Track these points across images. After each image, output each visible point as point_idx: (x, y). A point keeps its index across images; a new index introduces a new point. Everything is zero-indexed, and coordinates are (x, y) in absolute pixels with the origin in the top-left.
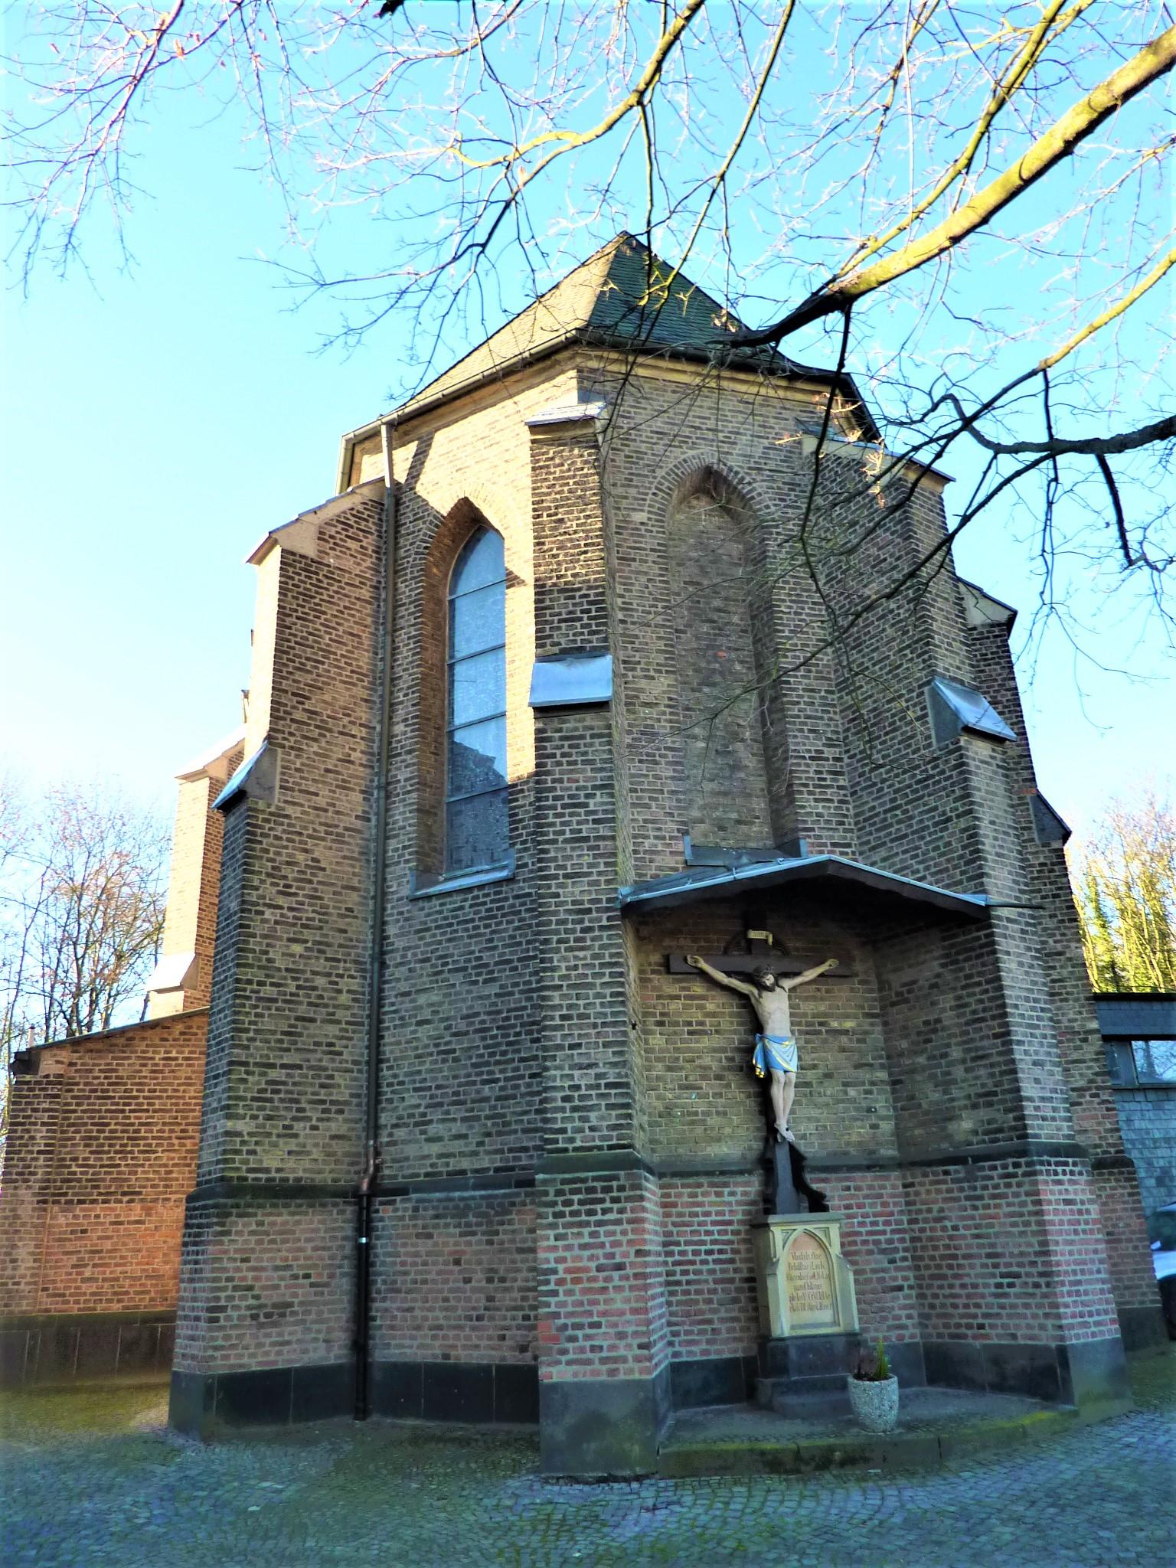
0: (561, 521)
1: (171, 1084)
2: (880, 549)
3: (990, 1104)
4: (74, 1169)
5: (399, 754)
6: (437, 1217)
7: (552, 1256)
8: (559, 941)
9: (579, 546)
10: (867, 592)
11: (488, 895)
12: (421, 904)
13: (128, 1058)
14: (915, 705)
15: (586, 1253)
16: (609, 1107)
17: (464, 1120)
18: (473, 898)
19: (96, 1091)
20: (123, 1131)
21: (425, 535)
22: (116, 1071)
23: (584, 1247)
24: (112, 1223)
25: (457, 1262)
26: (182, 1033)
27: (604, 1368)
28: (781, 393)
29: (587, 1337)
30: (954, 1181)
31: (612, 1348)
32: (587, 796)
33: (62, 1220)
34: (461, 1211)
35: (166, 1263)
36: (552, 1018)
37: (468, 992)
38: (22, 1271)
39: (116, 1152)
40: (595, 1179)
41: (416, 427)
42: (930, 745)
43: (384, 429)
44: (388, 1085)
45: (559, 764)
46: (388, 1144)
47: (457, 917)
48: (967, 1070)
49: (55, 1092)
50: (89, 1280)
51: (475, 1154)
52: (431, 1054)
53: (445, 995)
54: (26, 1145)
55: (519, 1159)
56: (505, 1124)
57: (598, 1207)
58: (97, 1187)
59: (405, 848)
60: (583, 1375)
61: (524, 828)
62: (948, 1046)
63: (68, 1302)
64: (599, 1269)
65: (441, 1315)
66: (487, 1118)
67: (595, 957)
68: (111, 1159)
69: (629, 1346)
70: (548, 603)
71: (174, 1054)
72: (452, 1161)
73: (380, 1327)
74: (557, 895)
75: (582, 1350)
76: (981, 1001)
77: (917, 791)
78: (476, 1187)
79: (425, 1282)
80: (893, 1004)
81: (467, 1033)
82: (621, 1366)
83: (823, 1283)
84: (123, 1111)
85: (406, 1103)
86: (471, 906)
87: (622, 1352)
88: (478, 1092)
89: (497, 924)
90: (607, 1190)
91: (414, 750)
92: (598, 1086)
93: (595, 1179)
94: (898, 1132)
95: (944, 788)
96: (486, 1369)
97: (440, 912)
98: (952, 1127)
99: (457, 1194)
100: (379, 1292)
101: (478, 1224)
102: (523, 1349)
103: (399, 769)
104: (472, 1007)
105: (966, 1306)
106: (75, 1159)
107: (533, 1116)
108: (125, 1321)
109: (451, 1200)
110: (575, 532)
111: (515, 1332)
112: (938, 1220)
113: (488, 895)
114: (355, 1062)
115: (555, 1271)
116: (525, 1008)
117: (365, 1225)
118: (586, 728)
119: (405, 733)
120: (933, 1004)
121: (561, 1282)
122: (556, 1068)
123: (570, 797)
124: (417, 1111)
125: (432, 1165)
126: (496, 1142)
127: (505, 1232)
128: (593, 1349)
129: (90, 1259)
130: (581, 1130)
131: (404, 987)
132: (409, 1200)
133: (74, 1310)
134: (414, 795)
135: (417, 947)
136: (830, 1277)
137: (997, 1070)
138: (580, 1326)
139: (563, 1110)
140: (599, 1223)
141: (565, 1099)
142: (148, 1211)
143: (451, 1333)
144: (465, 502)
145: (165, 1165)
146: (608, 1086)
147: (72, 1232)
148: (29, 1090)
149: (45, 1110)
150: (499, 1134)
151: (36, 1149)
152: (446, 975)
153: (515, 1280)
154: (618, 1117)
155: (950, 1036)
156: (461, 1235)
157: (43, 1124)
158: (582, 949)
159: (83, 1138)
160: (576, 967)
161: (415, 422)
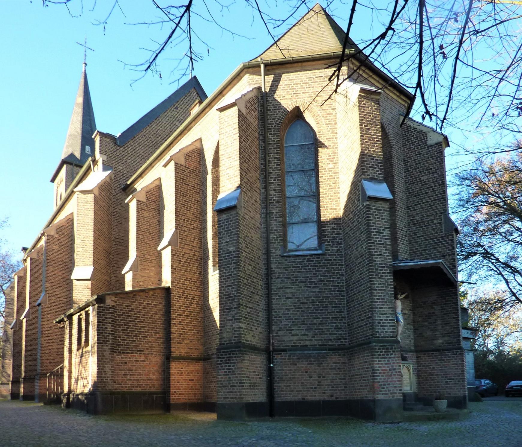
0: (368, 129)
1: (150, 313)
2: (430, 165)
3: (449, 336)
4: (120, 341)
5: (273, 203)
6: (299, 359)
7: (378, 366)
8: (376, 275)
9: (374, 141)
10: (422, 178)
11: (314, 258)
12: (286, 258)
13: (135, 302)
14: (438, 219)
15: (387, 365)
16: (391, 326)
17: (306, 330)
18: (308, 259)
19: (124, 313)
20: (136, 329)
21: (280, 117)
22: (130, 306)
23: (386, 364)
25: (307, 372)
26: (153, 295)
27: (391, 395)
28: (395, 97)
29: (387, 388)
30: (435, 356)
31: (393, 390)
32: (383, 230)
33: (118, 359)
34: (307, 357)
35: (153, 375)
36: (374, 299)
37: (307, 290)
38: (108, 375)
40: (388, 345)
41: (274, 69)
42: (442, 232)
43: (262, 66)
45: (375, 218)
46: (276, 336)
48: (442, 327)
51: (311, 340)
52: (293, 308)
53: (297, 290)
54: (104, 331)
55: (328, 342)
56: (322, 332)
57: (389, 353)
58: (129, 348)
59: (277, 237)
60: (386, 397)
61: (328, 237)
63: (122, 387)
64: (390, 370)
66: (316, 329)
67: (386, 281)
68: (132, 338)
69: (397, 390)
70: (365, 159)
71: (150, 303)
72: (302, 342)
73: (277, 391)
74: (375, 261)
75: (386, 391)
76: (450, 308)
77: (435, 246)
78: (313, 350)
79: (294, 378)
80: (418, 307)
81: (307, 303)
82: (395, 395)
83: (408, 380)
84: (135, 321)
85: (283, 324)
86: (307, 261)
87: (395, 391)
88: (312, 321)
89: (318, 269)
90: (392, 349)
91: (280, 202)
92: (387, 320)
93: (388, 345)
94: (415, 343)
95: (445, 246)
96: (319, 402)
97: (295, 262)
98: (435, 342)
100: (276, 381)
101: (314, 361)
104: (308, 295)
105: (434, 387)
106: (120, 337)
107: (333, 330)
108: (143, 394)
109: (304, 354)
110: (373, 135)
111: (329, 391)
112: (428, 366)
113: (314, 258)
114: (263, 309)
115: (378, 370)
116: (330, 297)
117: (270, 360)
118: (382, 207)
119: (275, 195)
120: (433, 308)
121: (380, 373)
122: (376, 314)
123: (378, 229)
124: (287, 326)
125: (294, 343)
126: (320, 337)
127: (325, 363)
128: (389, 390)
129: (129, 373)
130: (383, 332)
131: (279, 286)
132: (286, 354)
133: (125, 389)
134: (281, 219)
135: (285, 273)
136: (410, 378)
137: (452, 327)
138: (385, 385)
139: (378, 326)
140: (390, 358)
141: (379, 323)
142: (146, 358)
143: (305, 392)
144: (297, 108)
145: (151, 342)
146: (390, 320)
147: (122, 363)
148: (103, 310)
150: (320, 334)
151: (108, 332)
152: (297, 283)
153: (329, 377)
154: (393, 329)
155: (437, 317)
156: (308, 364)
157: (110, 323)
158: (382, 279)
159: (122, 330)
160: (381, 284)
161: (274, 67)
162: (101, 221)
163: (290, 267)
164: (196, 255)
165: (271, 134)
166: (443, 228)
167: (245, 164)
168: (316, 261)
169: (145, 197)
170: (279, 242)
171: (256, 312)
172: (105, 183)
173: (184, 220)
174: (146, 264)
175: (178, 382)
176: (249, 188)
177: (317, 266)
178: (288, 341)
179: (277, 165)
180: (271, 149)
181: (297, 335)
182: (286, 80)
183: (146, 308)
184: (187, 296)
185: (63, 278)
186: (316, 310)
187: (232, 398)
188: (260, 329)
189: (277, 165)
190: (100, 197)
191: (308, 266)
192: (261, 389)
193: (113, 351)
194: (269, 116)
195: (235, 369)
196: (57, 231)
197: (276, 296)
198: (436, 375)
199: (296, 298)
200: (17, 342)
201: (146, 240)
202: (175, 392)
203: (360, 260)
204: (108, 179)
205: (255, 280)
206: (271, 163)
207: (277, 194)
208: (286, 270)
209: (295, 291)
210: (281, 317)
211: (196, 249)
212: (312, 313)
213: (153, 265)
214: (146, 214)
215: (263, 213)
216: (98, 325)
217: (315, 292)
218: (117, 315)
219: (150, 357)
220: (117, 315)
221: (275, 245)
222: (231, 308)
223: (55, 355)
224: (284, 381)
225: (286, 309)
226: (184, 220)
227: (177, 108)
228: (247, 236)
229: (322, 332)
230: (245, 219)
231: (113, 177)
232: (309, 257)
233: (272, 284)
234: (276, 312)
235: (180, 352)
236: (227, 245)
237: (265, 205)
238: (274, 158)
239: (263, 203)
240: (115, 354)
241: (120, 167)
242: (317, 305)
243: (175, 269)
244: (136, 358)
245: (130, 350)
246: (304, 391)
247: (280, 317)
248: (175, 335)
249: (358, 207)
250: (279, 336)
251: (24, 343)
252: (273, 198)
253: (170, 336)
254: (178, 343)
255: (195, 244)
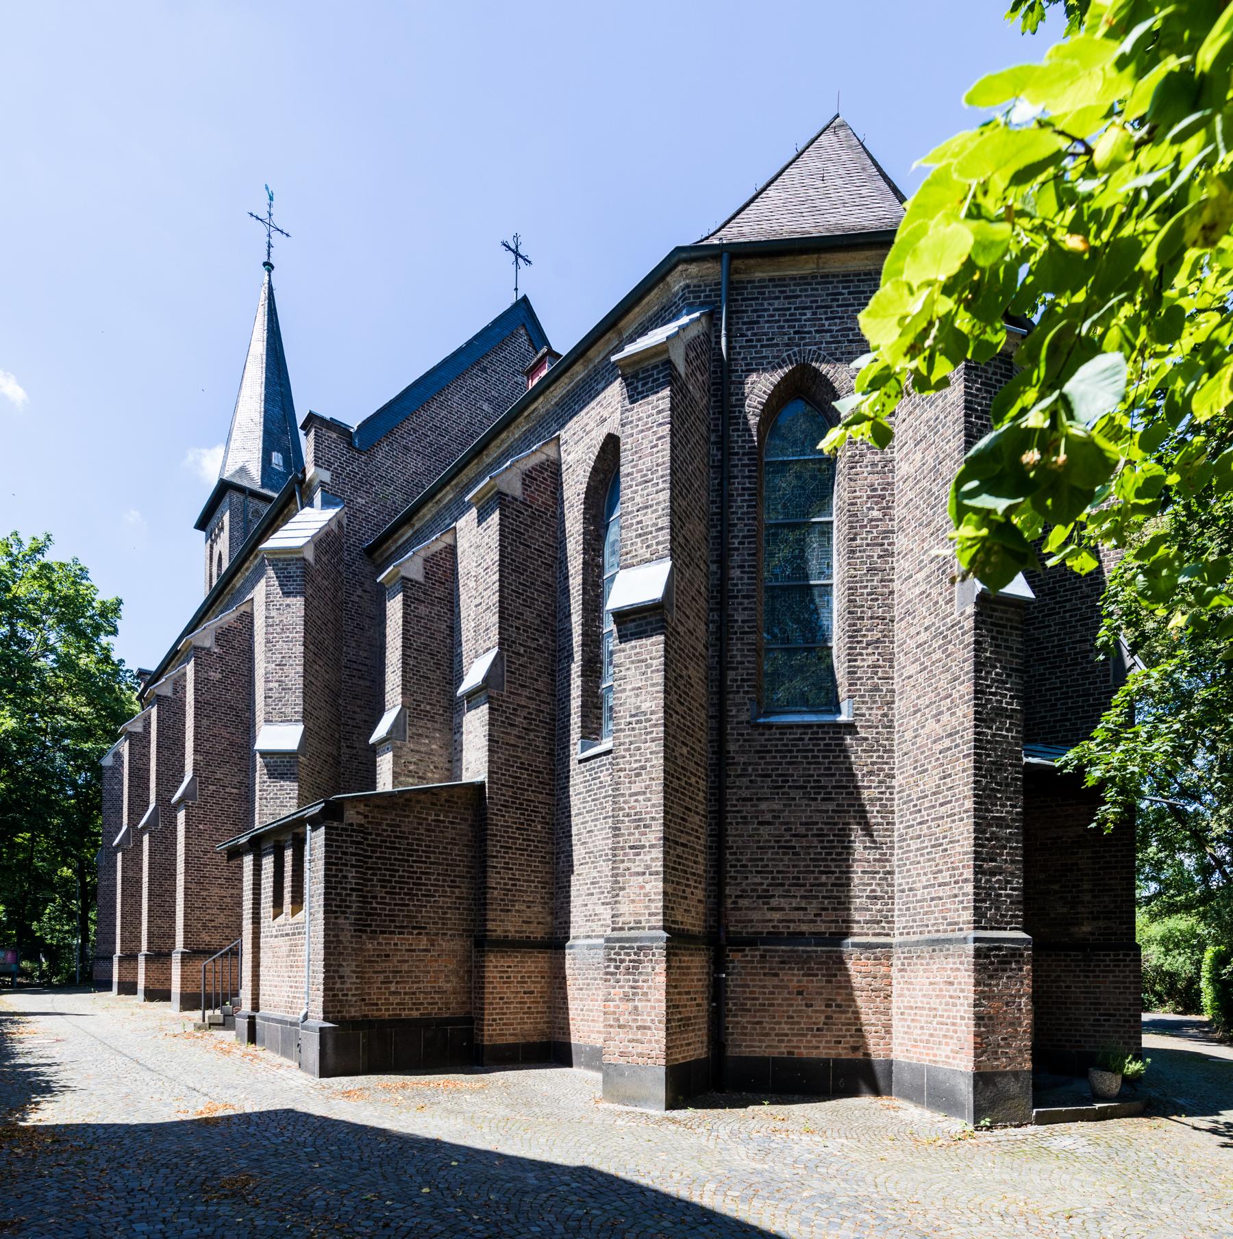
1: (441, 842)
5: (737, 597)
6: (783, 962)
13: (408, 816)
18: (812, 733)
19: (385, 841)
22: (399, 826)
24: (408, 950)
35: (447, 982)
39: (405, 894)
42: (1108, 681)
44: (731, 866)
46: (732, 909)
47: (796, 745)
49: (359, 839)
50: (394, 993)
52: (773, 847)
53: (785, 805)
54: (341, 883)
58: (394, 921)
59: (743, 680)
62: (1082, 880)
65: (786, 1027)
66: (823, 897)
68: (402, 899)
71: (442, 818)
72: (792, 925)
73: (732, 1034)
77: (1088, 711)
84: (408, 861)
86: (810, 739)
88: (816, 878)
89: (834, 757)
91: (753, 597)
98: (1073, 930)
99: (801, 948)
102: (855, 1049)
103: (736, 610)
106: (375, 897)
108: (424, 1023)
117: (718, 963)
118: (1008, 620)
119: (742, 579)
124: (759, 888)
131: (745, 793)
143: (795, 1039)
145: (441, 907)
148: (337, 835)
149: (353, 854)
150: (834, 909)
157: (352, 866)
159: (379, 881)
162: (319, 622)
163: (770, 752)
164: (542, 712)
165: (738, 430)
166: (1111, 672)
167: (680, 499)
168: (830, 739)
169: (422, 571)
170: (747, 692)
171: (693, 855)
172: (327, 534)
173: (518, 628)
174: (421, 723)
175: (501, 998)
176: (687, 560)
177: (835, 751)
178: (758, 921)
179: (748, 507)
180: (736, 466)
181: (782, 909)
182: (777, 298)
183: (434, 831)
184: (521, 804)
185: (231, 744)
186: (827, 854)
187: (640, 1055)
188: (700, 894)
189: (748, 507)
190: (318, 567)
191: (813, 751)
192: (699, 1030)
193: (360, 931)
194: (733, 387)
195: (649, 987)
196: (217, 639)
197: (736, 817)
198: (1072, 1003)
199: (782, 823)
200: (130, 874)
201: (424, 670)
202: (494, 1020)
203: (947, 743)
204: (334, 526)
205: (693, 780)
206: (736, 501)
207: (746, 576)
208: (760, 758)
209: (782, 807)
210: (746, 866)
211: (543, 697)
212: (818, 860)
213: (437, 726)
214: (423, 610)
215: (712, 622)
216: (326, 870)
217: (827, 811)
218: (368, 845)
219: (441, 942)
220: (368, 845)
221: (738, 698)
222: (643, 847)
223: (215, 911)
224: (749, 1010)
225: (758, 848)
226: (518, 628)
227: (484, 370)
228: (681, 676)
229: (839, 903)
230: (678, 633)
231: (345, 521)
232: (815, 729)
233: (728, 788)
234: (735, 853)
235: (506, 931)
236: (637, 696)
237: (717, 603)
238: (743, 489)
239: (712, 598)
240: (364, 936)
241: (359, 500)
242: (828, 841)
243: (497, 742)
244: (411, 945)
245: (396, 927)
246: (793, 1035)
247: (743, 866)
248: (496, 892)
249: (947, 616)
250: (740, 909)
251: (145, 879)
252: (736, 585)
253: (486, 893)
254: (502, 910)
255: (540, 685)
